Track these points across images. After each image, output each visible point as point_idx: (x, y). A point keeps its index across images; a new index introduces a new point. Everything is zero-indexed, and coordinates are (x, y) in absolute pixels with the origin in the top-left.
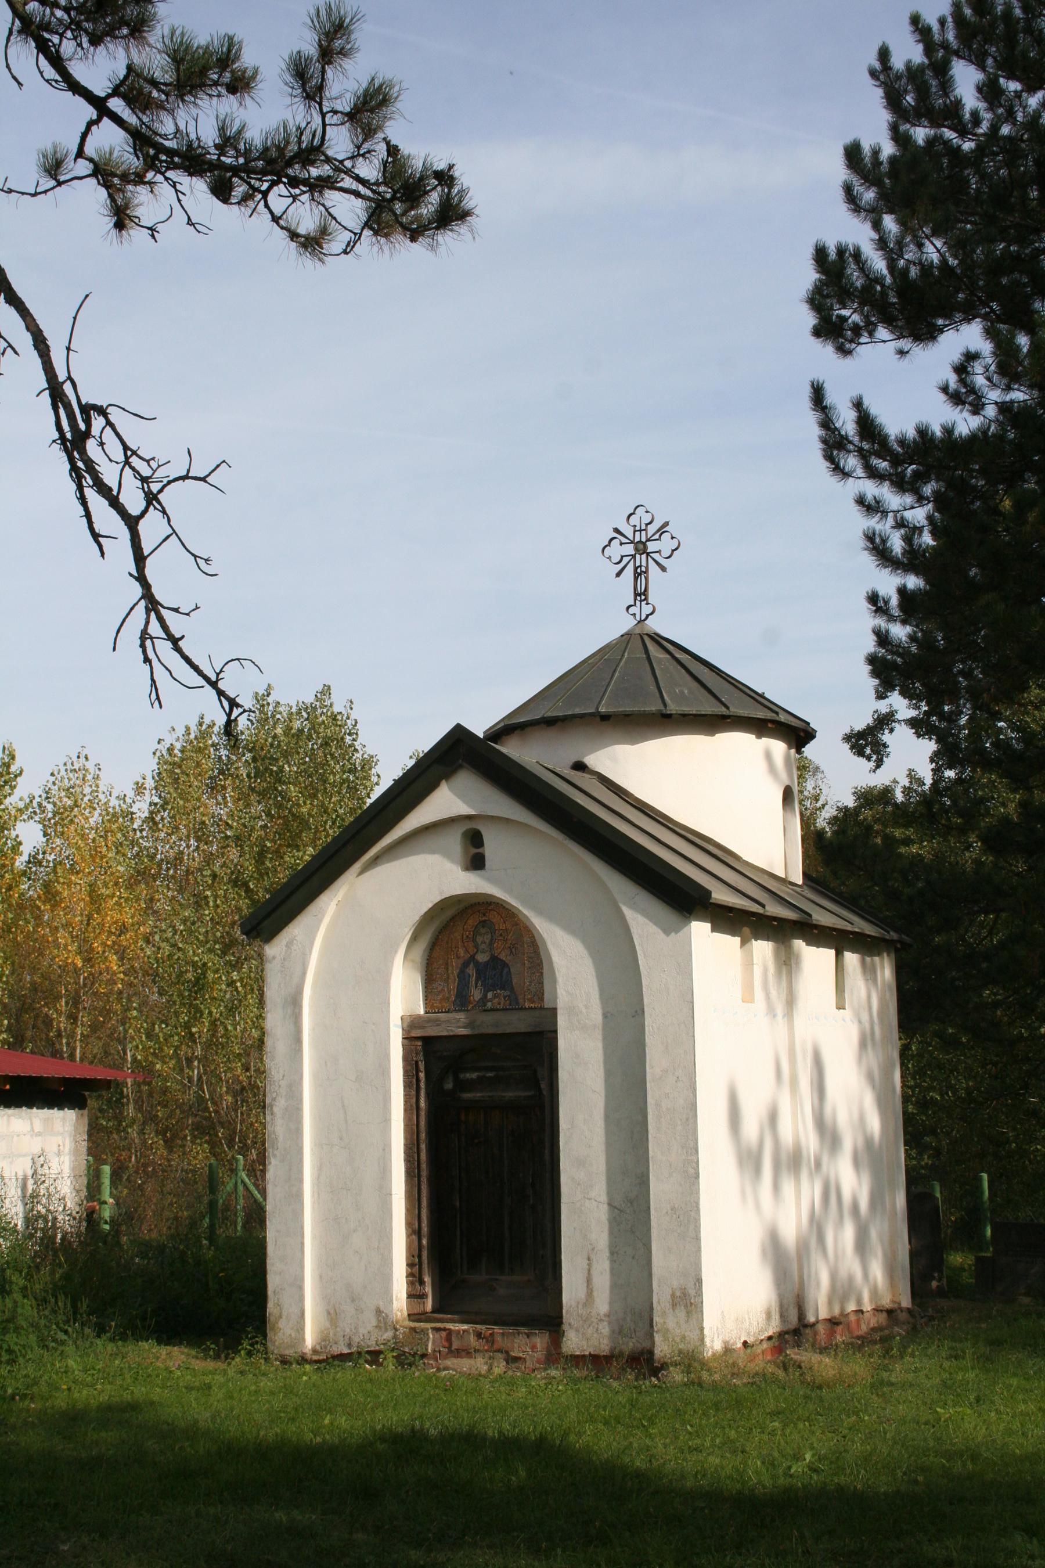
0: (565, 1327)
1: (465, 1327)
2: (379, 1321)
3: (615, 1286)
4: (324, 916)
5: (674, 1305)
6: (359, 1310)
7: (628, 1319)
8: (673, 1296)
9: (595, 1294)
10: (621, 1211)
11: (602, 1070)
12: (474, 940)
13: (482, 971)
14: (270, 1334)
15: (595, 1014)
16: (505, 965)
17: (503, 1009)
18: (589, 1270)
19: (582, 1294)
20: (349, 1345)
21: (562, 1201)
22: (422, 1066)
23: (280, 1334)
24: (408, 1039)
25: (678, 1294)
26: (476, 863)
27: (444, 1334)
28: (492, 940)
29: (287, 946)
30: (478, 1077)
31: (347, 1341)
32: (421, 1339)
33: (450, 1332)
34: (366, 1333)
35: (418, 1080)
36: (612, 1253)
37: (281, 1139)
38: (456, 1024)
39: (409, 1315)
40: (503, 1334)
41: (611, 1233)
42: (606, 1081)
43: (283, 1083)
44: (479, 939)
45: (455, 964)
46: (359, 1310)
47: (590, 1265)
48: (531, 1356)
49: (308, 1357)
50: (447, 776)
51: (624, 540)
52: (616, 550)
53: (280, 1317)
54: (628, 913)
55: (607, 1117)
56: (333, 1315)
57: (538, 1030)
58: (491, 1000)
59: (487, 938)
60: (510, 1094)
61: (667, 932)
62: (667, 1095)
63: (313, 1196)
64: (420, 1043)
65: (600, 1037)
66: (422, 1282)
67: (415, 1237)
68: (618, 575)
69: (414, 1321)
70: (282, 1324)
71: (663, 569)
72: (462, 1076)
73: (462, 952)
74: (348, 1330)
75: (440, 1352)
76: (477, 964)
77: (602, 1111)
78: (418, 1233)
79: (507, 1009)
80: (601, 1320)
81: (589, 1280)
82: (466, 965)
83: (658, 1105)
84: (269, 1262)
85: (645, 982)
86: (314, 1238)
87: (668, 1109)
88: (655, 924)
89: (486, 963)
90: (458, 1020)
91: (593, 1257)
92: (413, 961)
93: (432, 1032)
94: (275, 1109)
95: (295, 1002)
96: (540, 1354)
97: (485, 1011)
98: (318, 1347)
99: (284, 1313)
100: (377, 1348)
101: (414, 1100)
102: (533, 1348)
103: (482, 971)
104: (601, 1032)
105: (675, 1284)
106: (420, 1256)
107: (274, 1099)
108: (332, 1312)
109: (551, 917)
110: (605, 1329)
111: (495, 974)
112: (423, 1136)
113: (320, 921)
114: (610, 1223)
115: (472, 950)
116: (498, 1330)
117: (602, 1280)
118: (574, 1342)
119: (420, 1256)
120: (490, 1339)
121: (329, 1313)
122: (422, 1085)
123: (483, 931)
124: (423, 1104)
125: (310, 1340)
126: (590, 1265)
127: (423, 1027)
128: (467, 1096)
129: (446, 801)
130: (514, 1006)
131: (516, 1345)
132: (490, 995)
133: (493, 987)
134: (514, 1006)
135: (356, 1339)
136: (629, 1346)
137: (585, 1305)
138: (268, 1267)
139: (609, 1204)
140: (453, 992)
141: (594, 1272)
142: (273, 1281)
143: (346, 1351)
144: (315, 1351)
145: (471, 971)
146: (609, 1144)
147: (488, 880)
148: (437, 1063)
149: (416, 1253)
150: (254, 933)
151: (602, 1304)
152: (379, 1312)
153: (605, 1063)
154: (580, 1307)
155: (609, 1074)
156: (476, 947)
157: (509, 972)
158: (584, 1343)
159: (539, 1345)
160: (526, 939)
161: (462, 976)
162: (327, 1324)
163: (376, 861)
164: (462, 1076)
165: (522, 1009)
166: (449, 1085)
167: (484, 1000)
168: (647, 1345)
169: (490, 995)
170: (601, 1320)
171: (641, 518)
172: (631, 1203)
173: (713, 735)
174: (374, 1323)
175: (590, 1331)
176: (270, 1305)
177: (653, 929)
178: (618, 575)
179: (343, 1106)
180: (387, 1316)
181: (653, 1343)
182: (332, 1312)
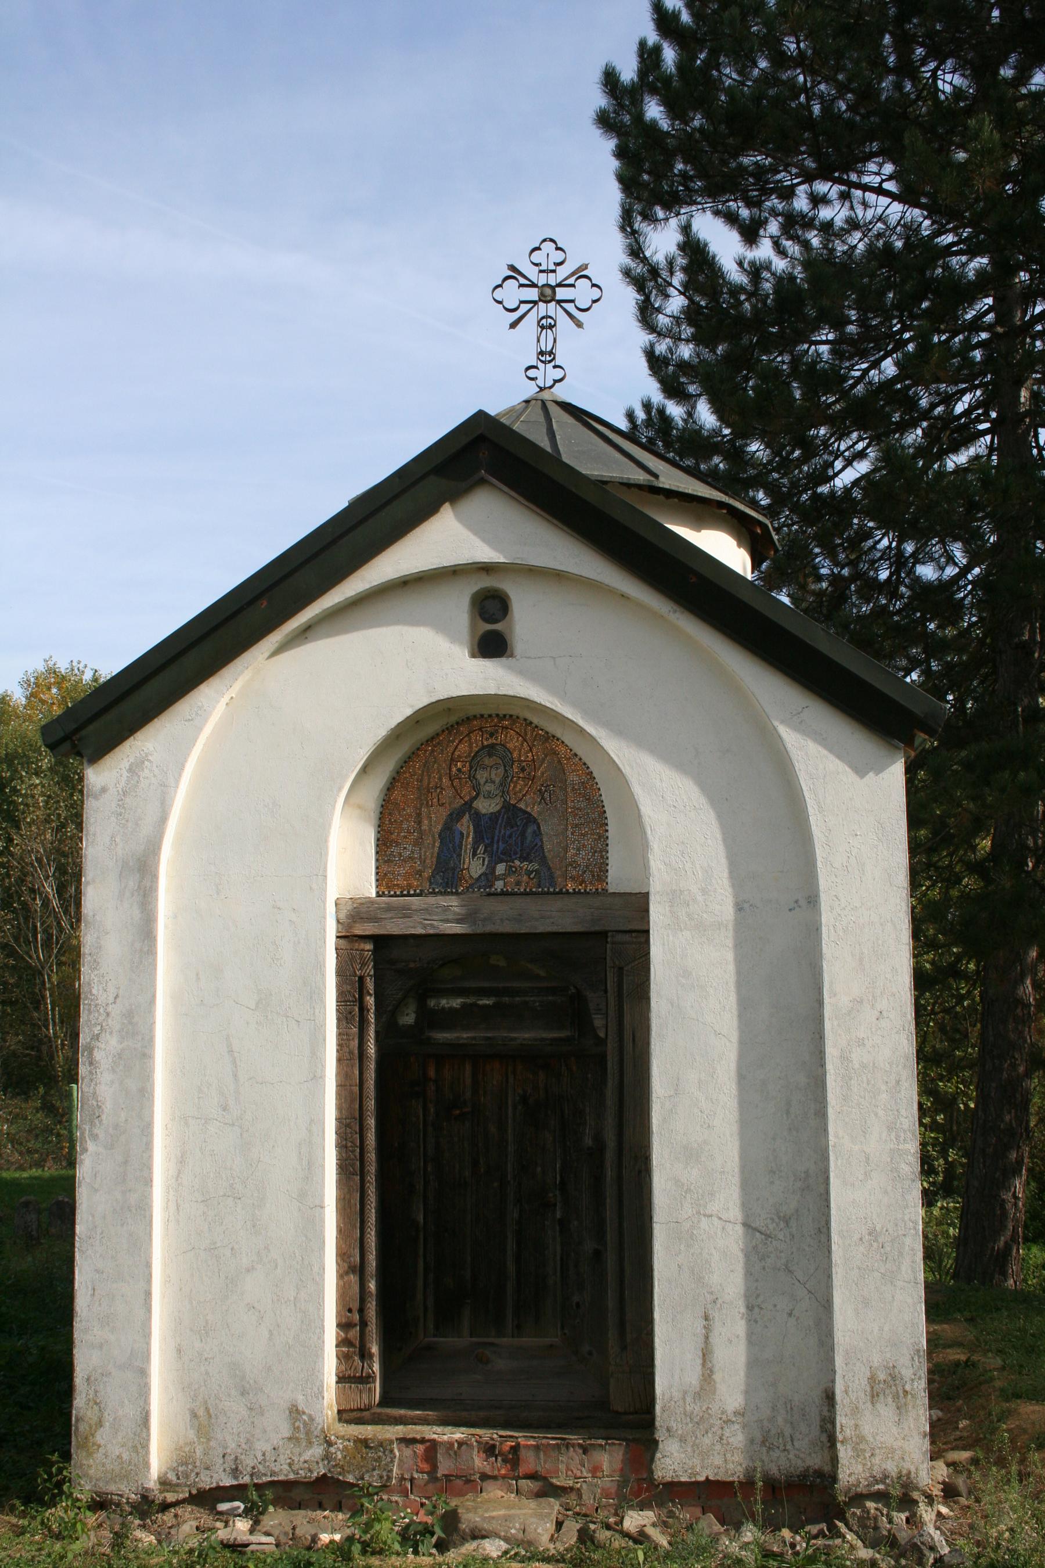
0: (660, 1435)
1: (458, 1434)
2: (297, 1429)
3: (753, 1364)
4: (206, 721)
5: (874, 1396)
6: (255, 1410)
7: (780, 1420)
8: (872, 1379)
9: (717, 1377)
10: (768, 1236)
11: (733, 998)
12: (472, 777)
13: (484, 827)
14: (77, 1455)
15: (722, 904)
16: (530, 819)
17: (525, 894)
18: (707, 1337)
19: (693, 1377)
20: (235, 1472)
21: (655, 1219)
22: (370, 985)
23: (99, 1456)
24: (347, 937)
25: (882, 1376)
26: (492, 645)
27: (420, 1448)
28: (505, 777)
29: (130, 770)
30: (464, 1006)
31: (230, 1464)
32: (379, 1459)
33: (432, 1446)
34: (272, 1449)
35: (363, 1009)
36: (750, 1308)
37: (108, 1107)
38: (442, 915)
39: (339, 1412)
40: (537, 1448)
41: (748, 1273)
42: (740, 1016)
43: (115, 1010)
44: (482, 776)
45: (435, 819)
46: (255, 1410)
47: (708, 1328)
48: (590, 1485)
49: (159, 1498)
50: (453, 497)
51: (523, 281)
52: (512, 294)
53: (100, 1424)
54: (788, 736)
55: (741, 1077)
56: (202, 1419)
57: (597, 928)
58: (502, 877)
59: (497, 775)
60: (525, 1035)
61: (861, 772)
62: (861, 1043)
63: (166, 1208)
64: (369, 946)
65: (730, 942)
66: (364, 1354)
67: (354, 1278)
68: (513, 325)
69: (349, 1422)
70: (102, 1437)
71: (579, 324)
72: (432, 1003)
73: (449, 793)
74: (232, 1445)
75: (412, 1480)
76: (477, 817)
77: (733, 1066)
78: (360, 1270)
79: (531, 893)
80: (728, 1422)
81: (706, 1354)
82: (455, 816)
83: (845, 1058)
84: (78, 1325)
85: (820, 853)
86: (167, 1281)
87: (864, 1066)
88: (839, 757)
89: (494, 817)
90: (446, 909)
91: (715, 1314)
92: (360, 807)
93: (394, 927)
94: (98, 1055)
95: (143, 868)
96: (608, 1481)
97: (489, 894)
98: (171, 1476)
99: (108, 1419)
100: (292, 1476)
101: (356, 1043)
102: (595, 1470)
103: (484, 827)
104: (730, 934)
105: (876, 1360)
106: (361, 1311)
107: (97, 1037)
108: (201, 1412)
109: (639, 741)
110: (737, 1437)
111: (510, 834)
112: (371, 1104)
113: (200, 729)
114: (747, 1256)
115: (467, 792)
116: (524, 1438)
117: (732, 1353)
118: (674, 1461)
119: (361, 1311)
120: (513, 1458)
121: (194, 1415)
122: (372, 1017)
123: (487, 761)
124: (371, 1049)
125: (157, 1463)
126: (708, 1328)
127: (375, 919)
128: (442, 1036)
129: (448, 538)
130: (545, 886)
131: (562, 1467)
132: (500, 869)
133: (506, 856)
134: (545, 886)
135: (248, 1462)
136: (782, 1463)
137: (698, 1396)
138: (77, 1335)
139: (746, 1225)
140: (431, 862)
141: (716, 1340)
142: (85, 1361)
143: (228, 1482)
144: (165, 1484)
145: (465, 825)
146: (744, 1123)
147: (522, 673)
148: (395, 983)
149: (355, 1306)
150: (66, 746)
151: (731, 1393)
152: (295, 1412)
153: (739, 985)
154: (689, 1399)
155: (745, 1006)
156: (477, 788)
157: (538, 833)
158: (697, 1461)
159: (605, 1466)
160: (573, 778)
161: (448, 835)
162: (192, 1434)
163: (306, 633)
164: (432, 1003)
165: (560, 892)
166: (408, 1018)
167: (489, 876)
168: (816, 1461)
169: (500, 869)
170: (728, 1422)
171: (548, 255)
172: (787, 1223)
173: (699, 531)
174: (286, 1431)
175: (707, 1441)
176: (79, 1401)
177: (834, 765)
178: (513, 325)
179: (231, 1051)
180: (312, 1419)
181: (834, 1460)
182: (201, 1412)
